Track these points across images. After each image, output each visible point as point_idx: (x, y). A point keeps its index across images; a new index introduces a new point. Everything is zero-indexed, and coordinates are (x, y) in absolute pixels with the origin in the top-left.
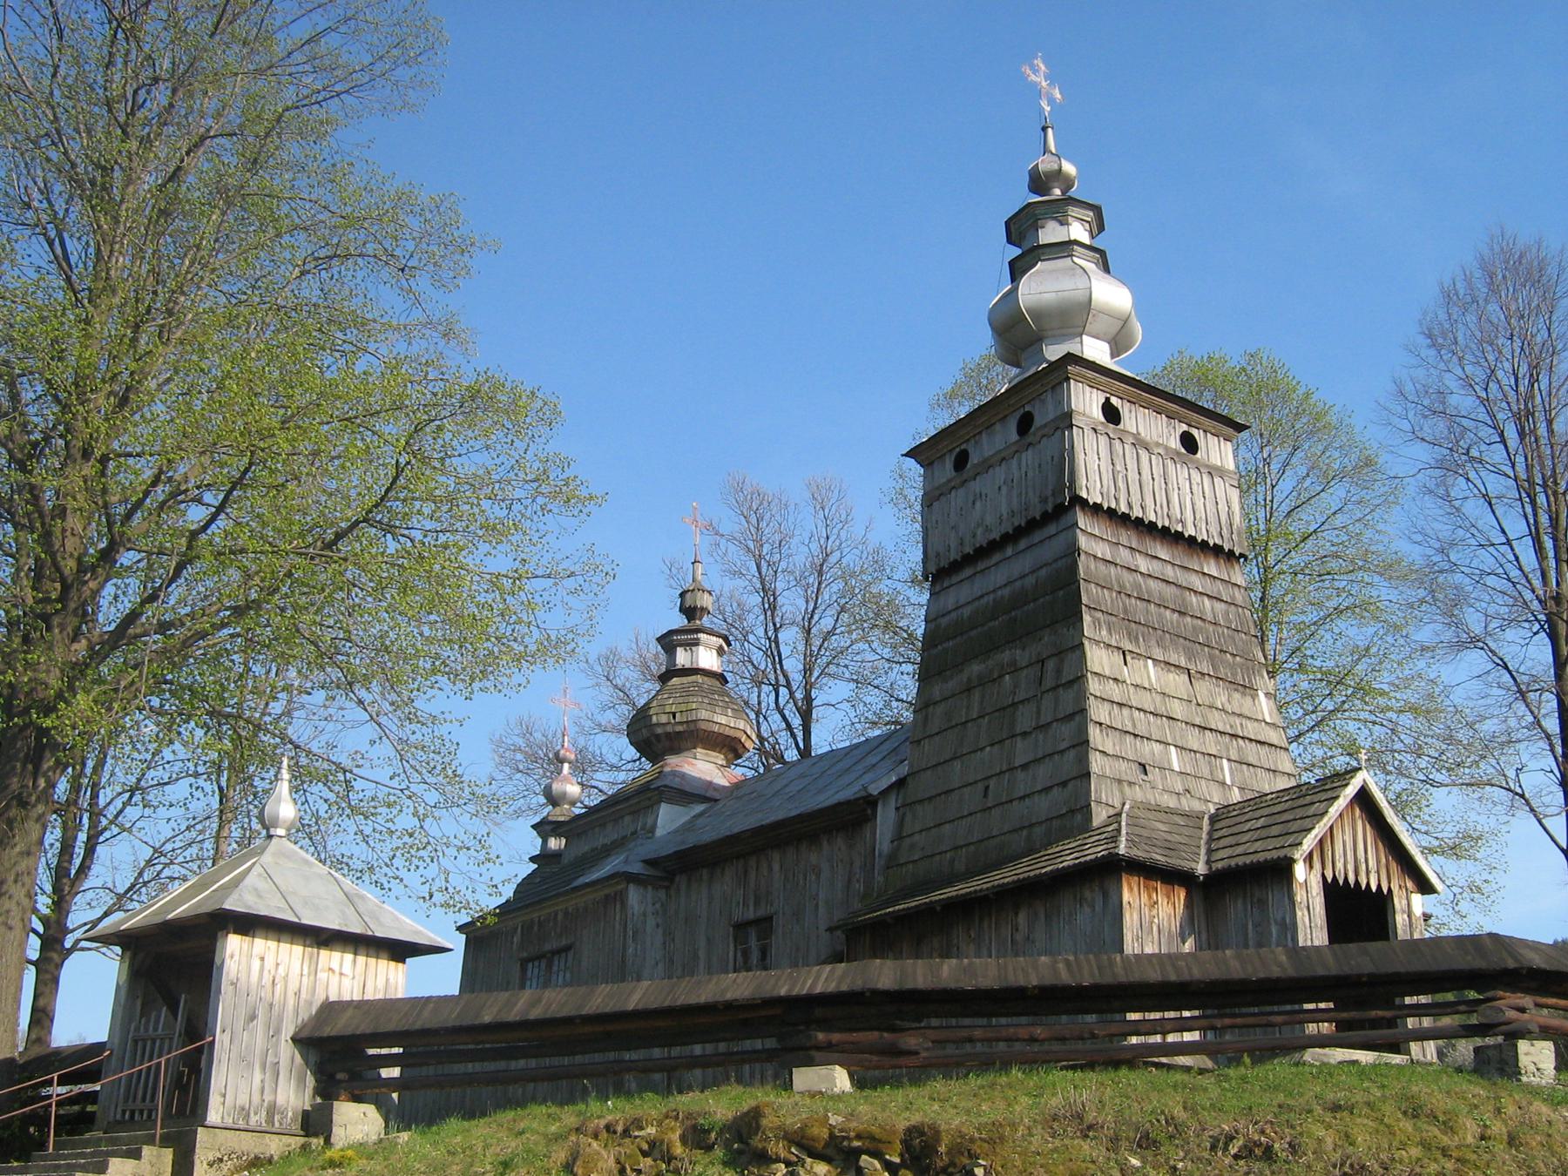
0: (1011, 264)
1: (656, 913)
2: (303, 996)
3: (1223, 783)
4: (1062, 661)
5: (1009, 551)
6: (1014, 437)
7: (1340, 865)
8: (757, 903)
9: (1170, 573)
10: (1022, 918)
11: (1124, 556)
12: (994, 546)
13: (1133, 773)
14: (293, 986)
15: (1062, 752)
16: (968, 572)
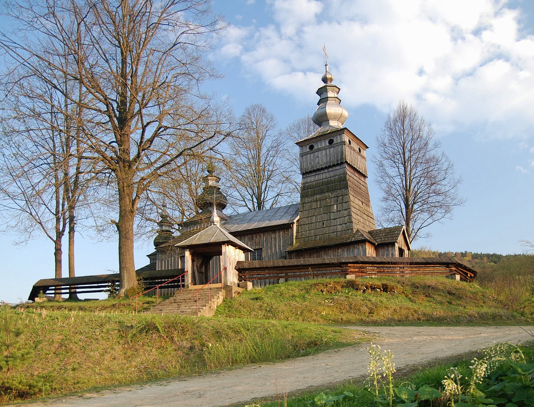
5: (326, 171)
6: (328, 144)
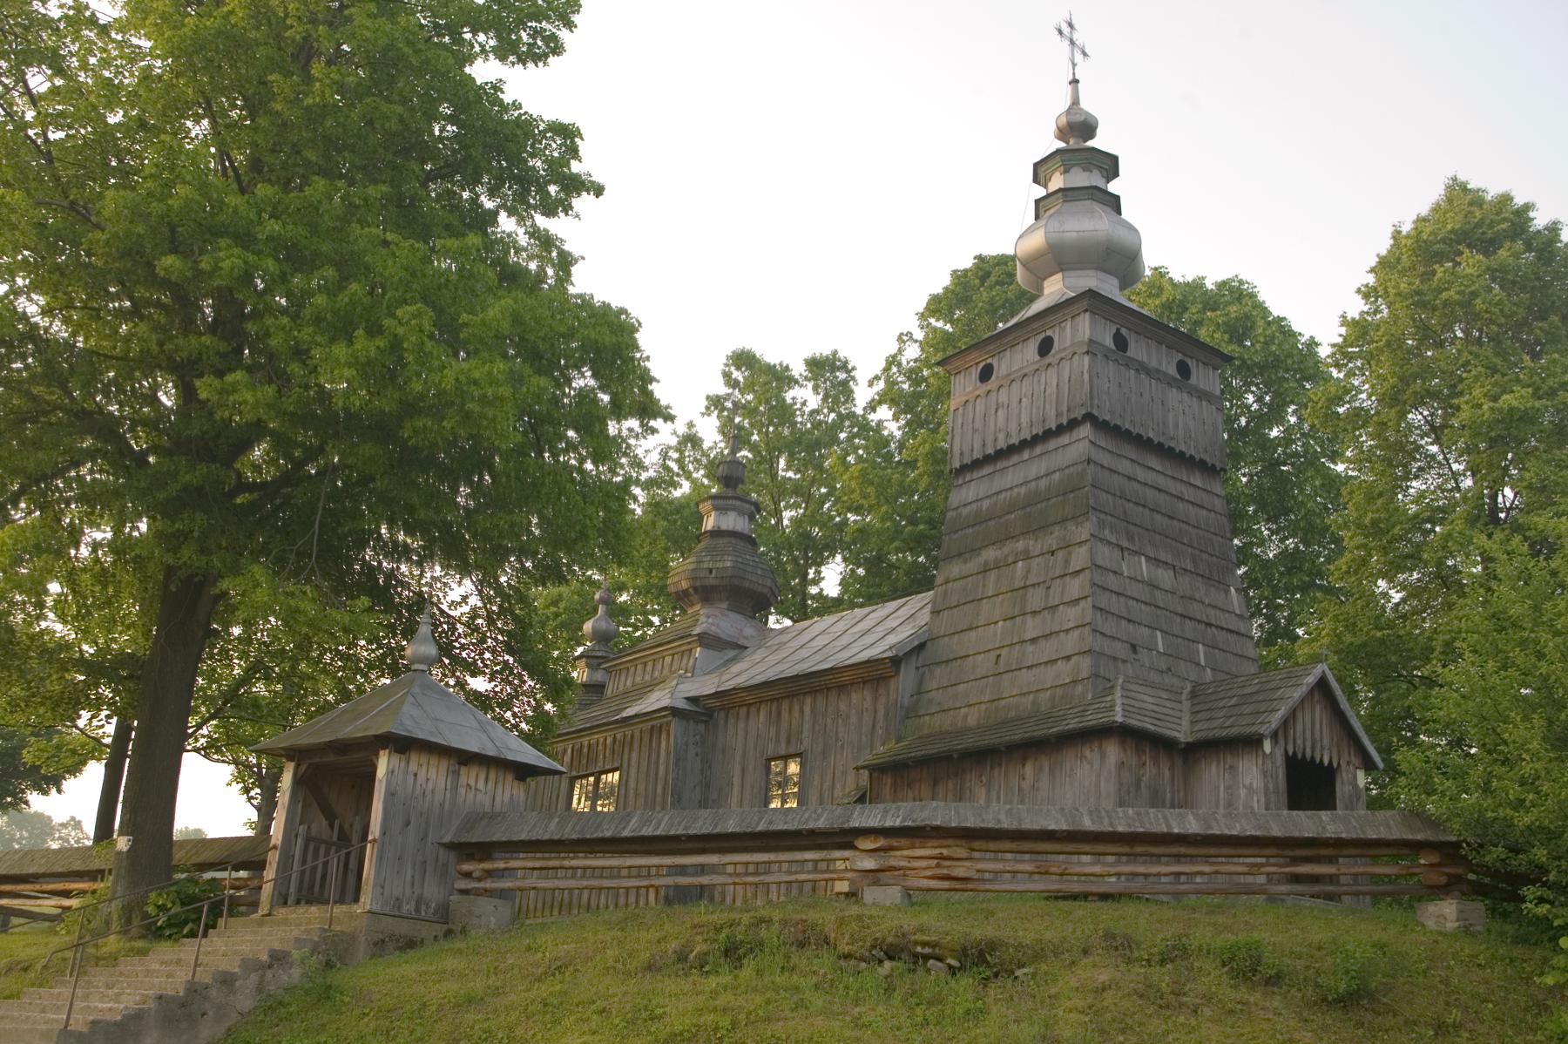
0: (1037, 202)
1: (696, 744)
2: (447, 806)
3: (1198, 664)
4: (1070, 553)
7: (1299, 742)
8: (788, 741)
9: (1162, 481)
10: (1029, 769)
11: (1125, 466)
12: (1011, 450)
13: (1121, 650)
14: (438, 798)
15: (1067, 631)
16: (987, 470)
